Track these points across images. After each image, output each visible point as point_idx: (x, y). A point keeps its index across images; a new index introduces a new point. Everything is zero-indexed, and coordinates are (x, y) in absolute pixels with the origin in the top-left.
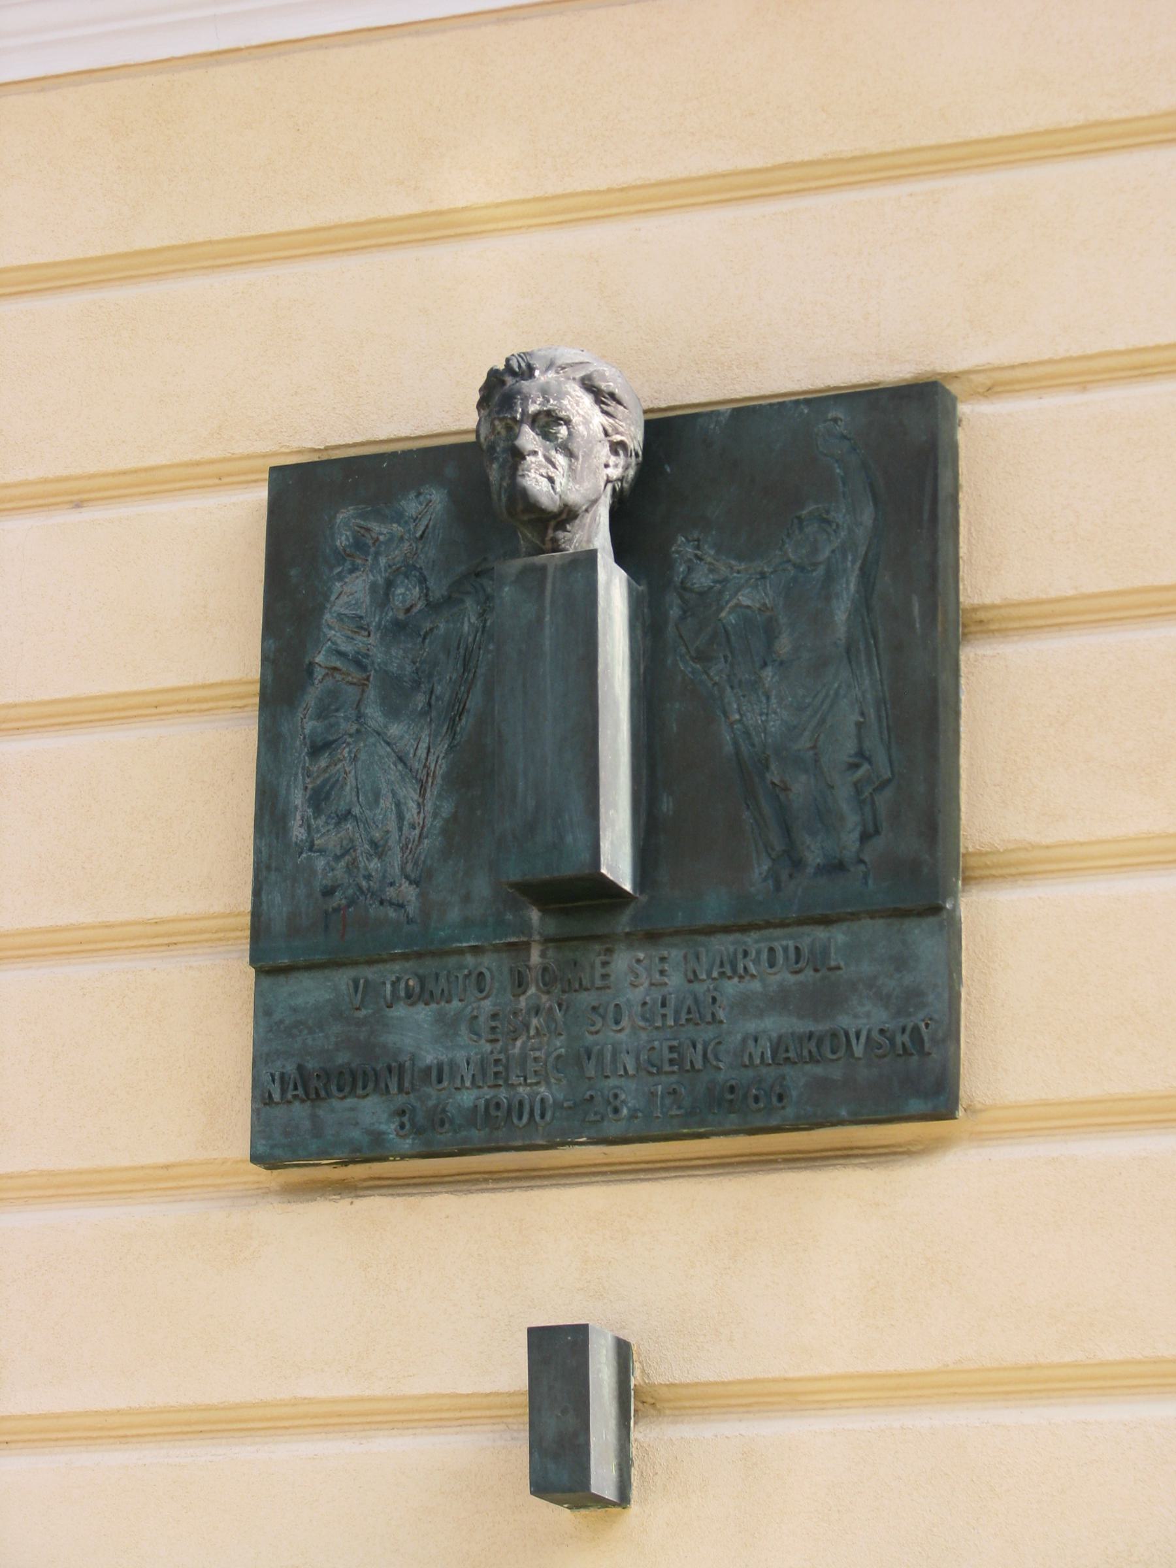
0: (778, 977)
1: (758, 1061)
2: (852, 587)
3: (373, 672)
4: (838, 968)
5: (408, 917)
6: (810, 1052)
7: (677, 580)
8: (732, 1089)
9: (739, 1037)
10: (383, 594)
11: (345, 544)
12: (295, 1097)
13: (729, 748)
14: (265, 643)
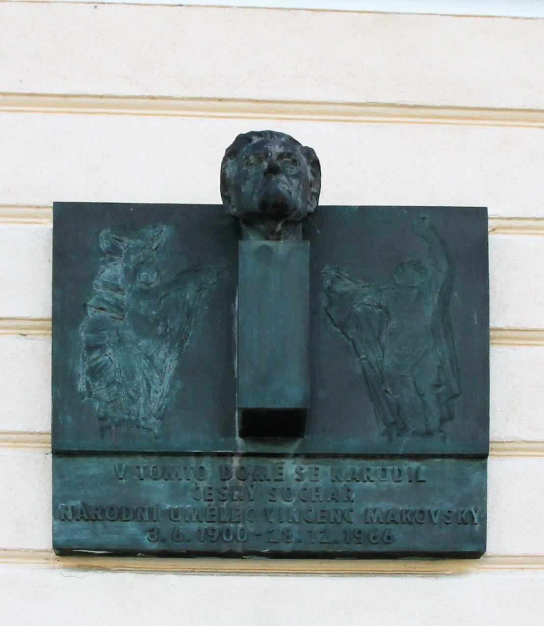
0: (387, 483)
1: (375, 521)
2: (436, 302)
3: (127, 313)
4: (424, 481)
5: (155, 435)
6: (407, 519)
7: (326, 287)
8: (360, 532)
9: (363, 510)
10: (132, 274)
11: (106, 247)
12: (82, 518)
13: (359, 371)
14: (55, 291)
